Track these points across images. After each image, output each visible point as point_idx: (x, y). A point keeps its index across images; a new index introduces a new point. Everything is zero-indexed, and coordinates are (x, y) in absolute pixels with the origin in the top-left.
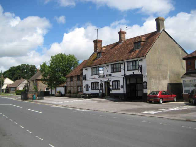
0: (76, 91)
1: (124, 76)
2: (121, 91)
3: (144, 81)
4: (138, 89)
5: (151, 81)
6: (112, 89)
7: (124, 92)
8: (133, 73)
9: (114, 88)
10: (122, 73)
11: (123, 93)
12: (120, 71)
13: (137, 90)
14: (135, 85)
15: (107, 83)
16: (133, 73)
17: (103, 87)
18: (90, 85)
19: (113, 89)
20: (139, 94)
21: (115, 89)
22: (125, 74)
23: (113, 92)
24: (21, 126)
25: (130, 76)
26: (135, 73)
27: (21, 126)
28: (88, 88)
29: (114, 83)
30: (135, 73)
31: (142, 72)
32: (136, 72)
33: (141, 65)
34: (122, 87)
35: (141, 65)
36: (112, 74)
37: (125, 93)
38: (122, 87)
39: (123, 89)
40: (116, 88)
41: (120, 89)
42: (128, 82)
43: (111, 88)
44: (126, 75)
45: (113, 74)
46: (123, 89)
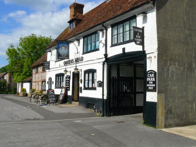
0: (40, 89)
1: (104, 59)
2: (98, 94)
3: (148, 70)
4: (137, 90)
5: (168, 70)
6: (83, 88)
7: (103, 95)
8: (124, 49)
9: (87, 86)
10: (100, 54)
11: (101, 97)
12: (98, 50)
13: (105, 58)
14: (126, 72)
15: (76, 75)
16: (124, 49)
17: (69, 83)
18: (54, 80)
19: (85, 89)
20: (139, 103)
21: (88, 89)
22: (106, 55)
23: (85, 94)
24: (134, 81)
25: (117, 58)
26: (126, 51)
27: (134, 81)
28: (51, 85)
29: (87, 75)
30: (126, 51)
31: (145, 45)
32: (132, 47)
33: (143, 27)
34: (101, 84)
35: (143, 27)
36: (84, 56)
37: (105, 98)
38: (101, 84)
39: (101, 88)
40: (90, 86)
41: (95, 89)
42: (114, 74)
43: (81, 85)
44: (109, 56)
45: (87, 57)
46: (101, 88)
